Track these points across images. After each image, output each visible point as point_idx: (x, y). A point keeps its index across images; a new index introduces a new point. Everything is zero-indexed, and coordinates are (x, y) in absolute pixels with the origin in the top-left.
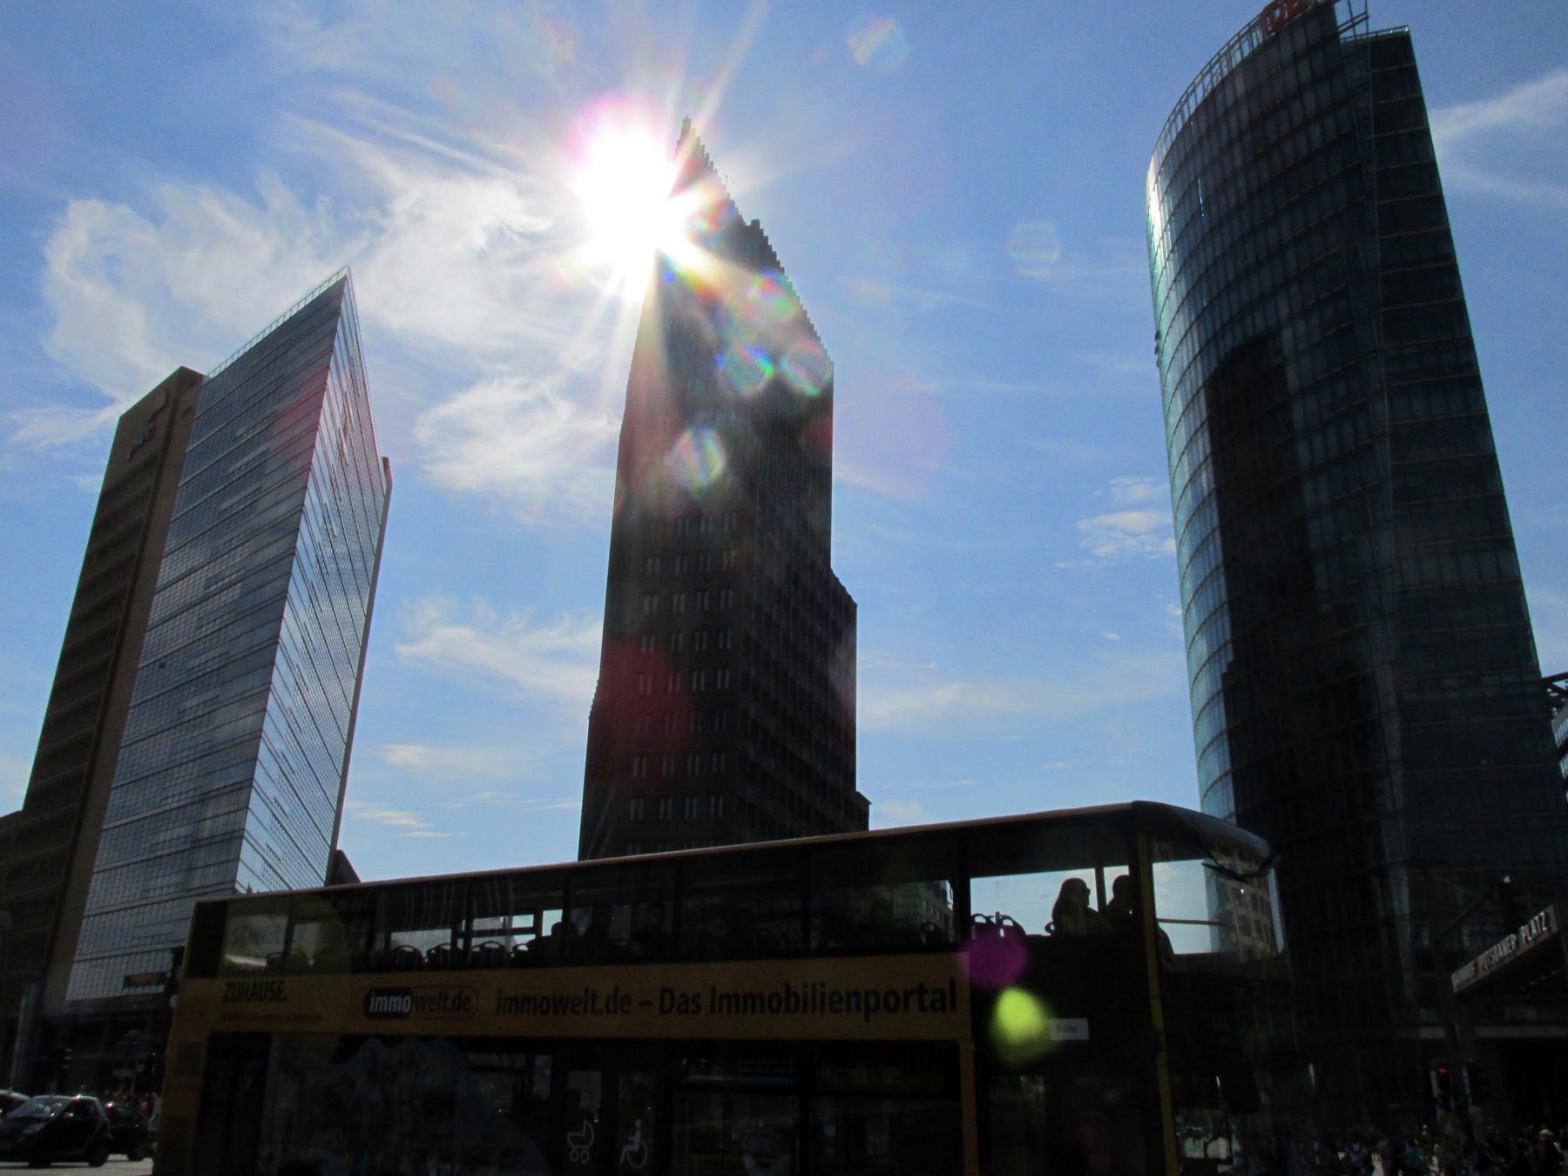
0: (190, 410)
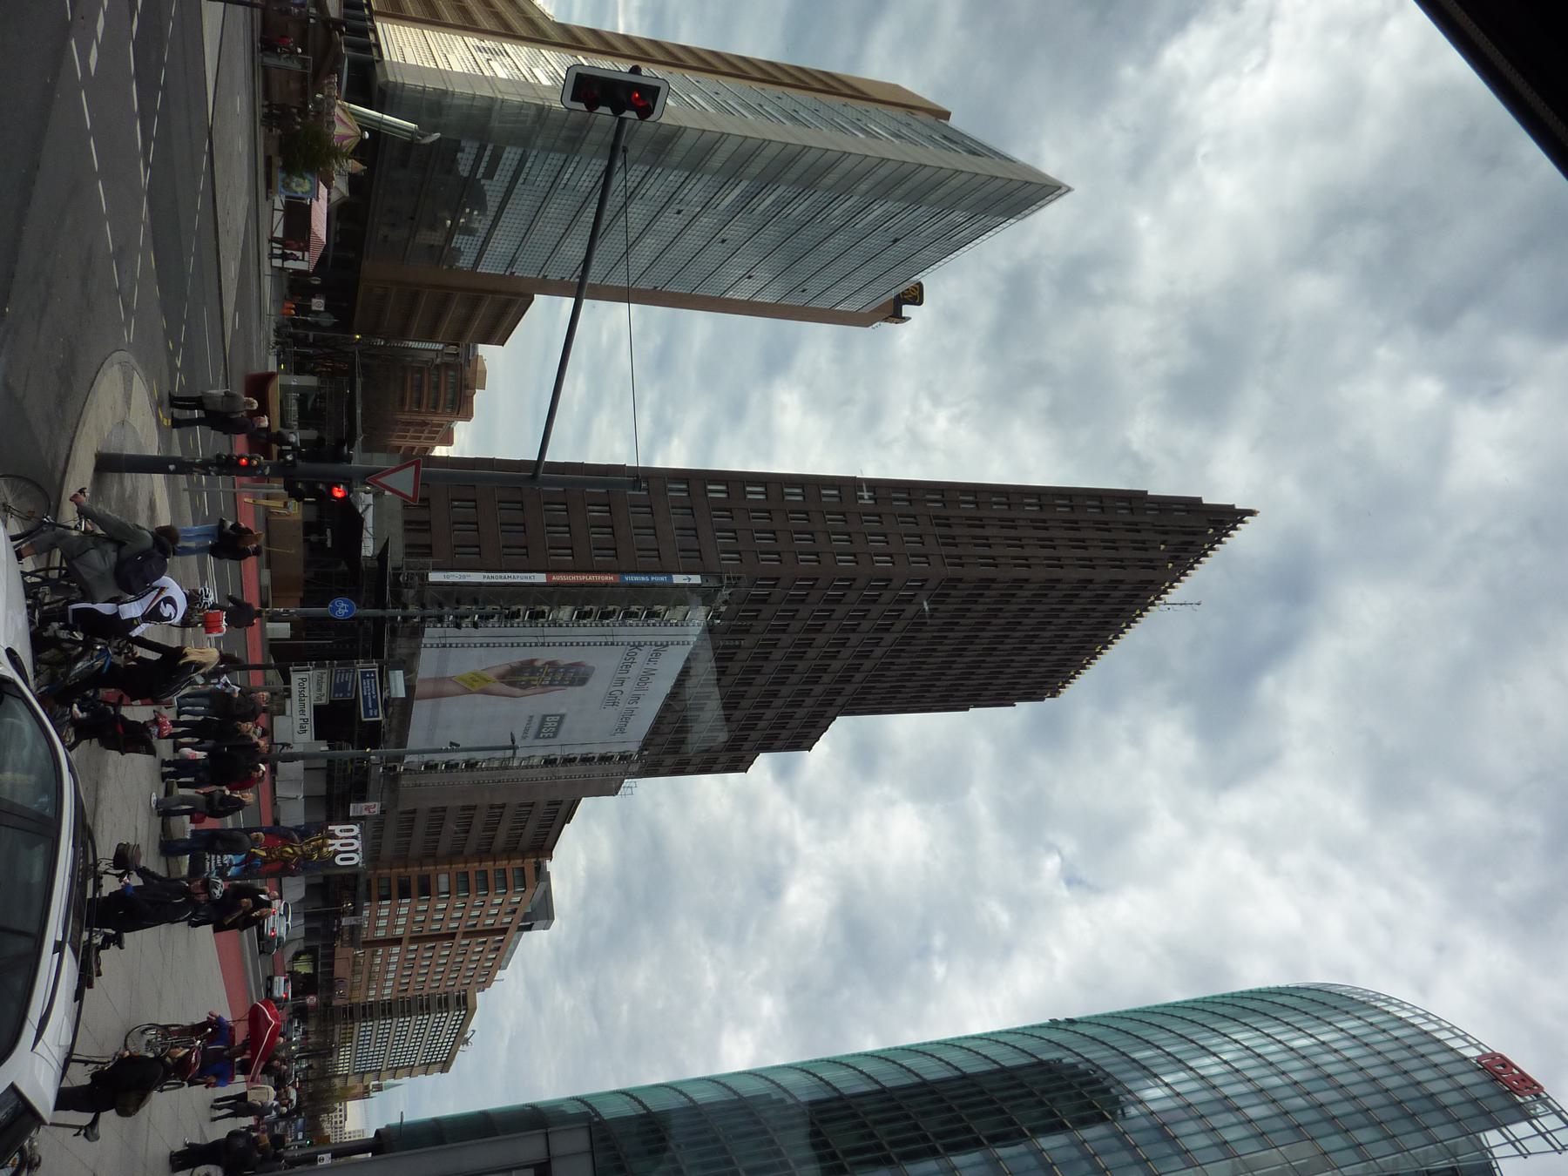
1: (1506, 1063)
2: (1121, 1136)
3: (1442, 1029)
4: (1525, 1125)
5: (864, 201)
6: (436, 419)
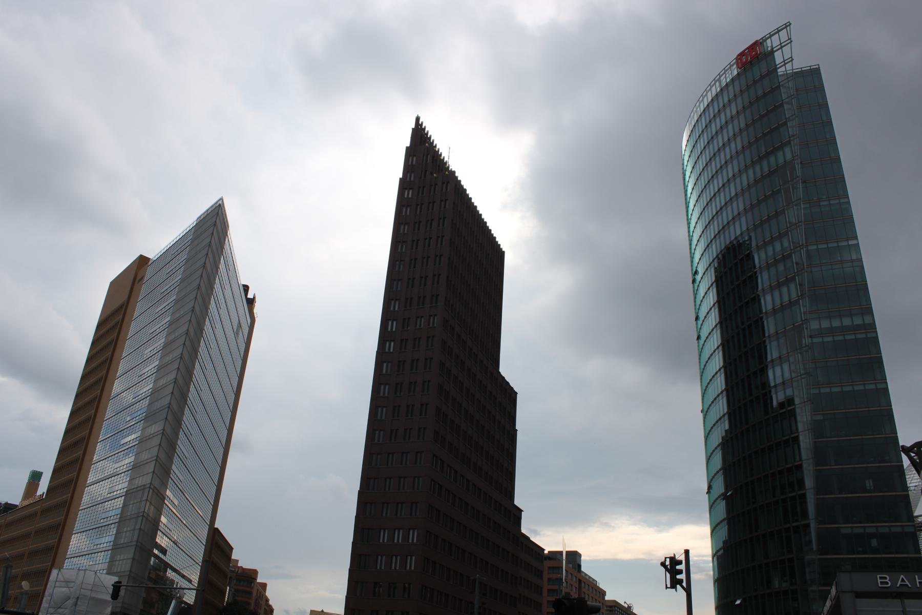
0: (142, 278)
1: (742, 54)
2: (768, 266)
3: (719, 80)
4: (776, 54)
5: (178, 312)
6: (254, 594)
